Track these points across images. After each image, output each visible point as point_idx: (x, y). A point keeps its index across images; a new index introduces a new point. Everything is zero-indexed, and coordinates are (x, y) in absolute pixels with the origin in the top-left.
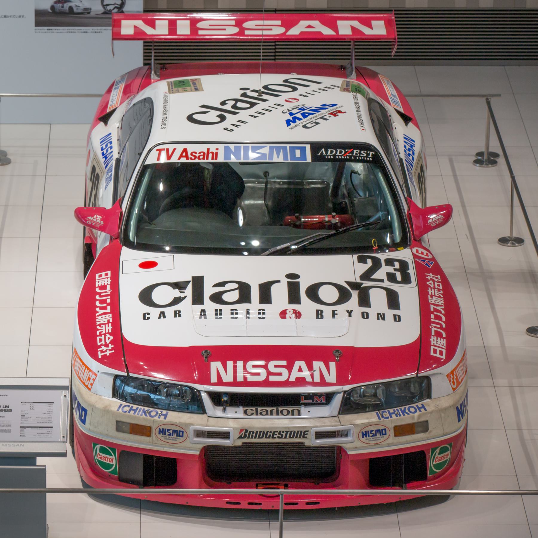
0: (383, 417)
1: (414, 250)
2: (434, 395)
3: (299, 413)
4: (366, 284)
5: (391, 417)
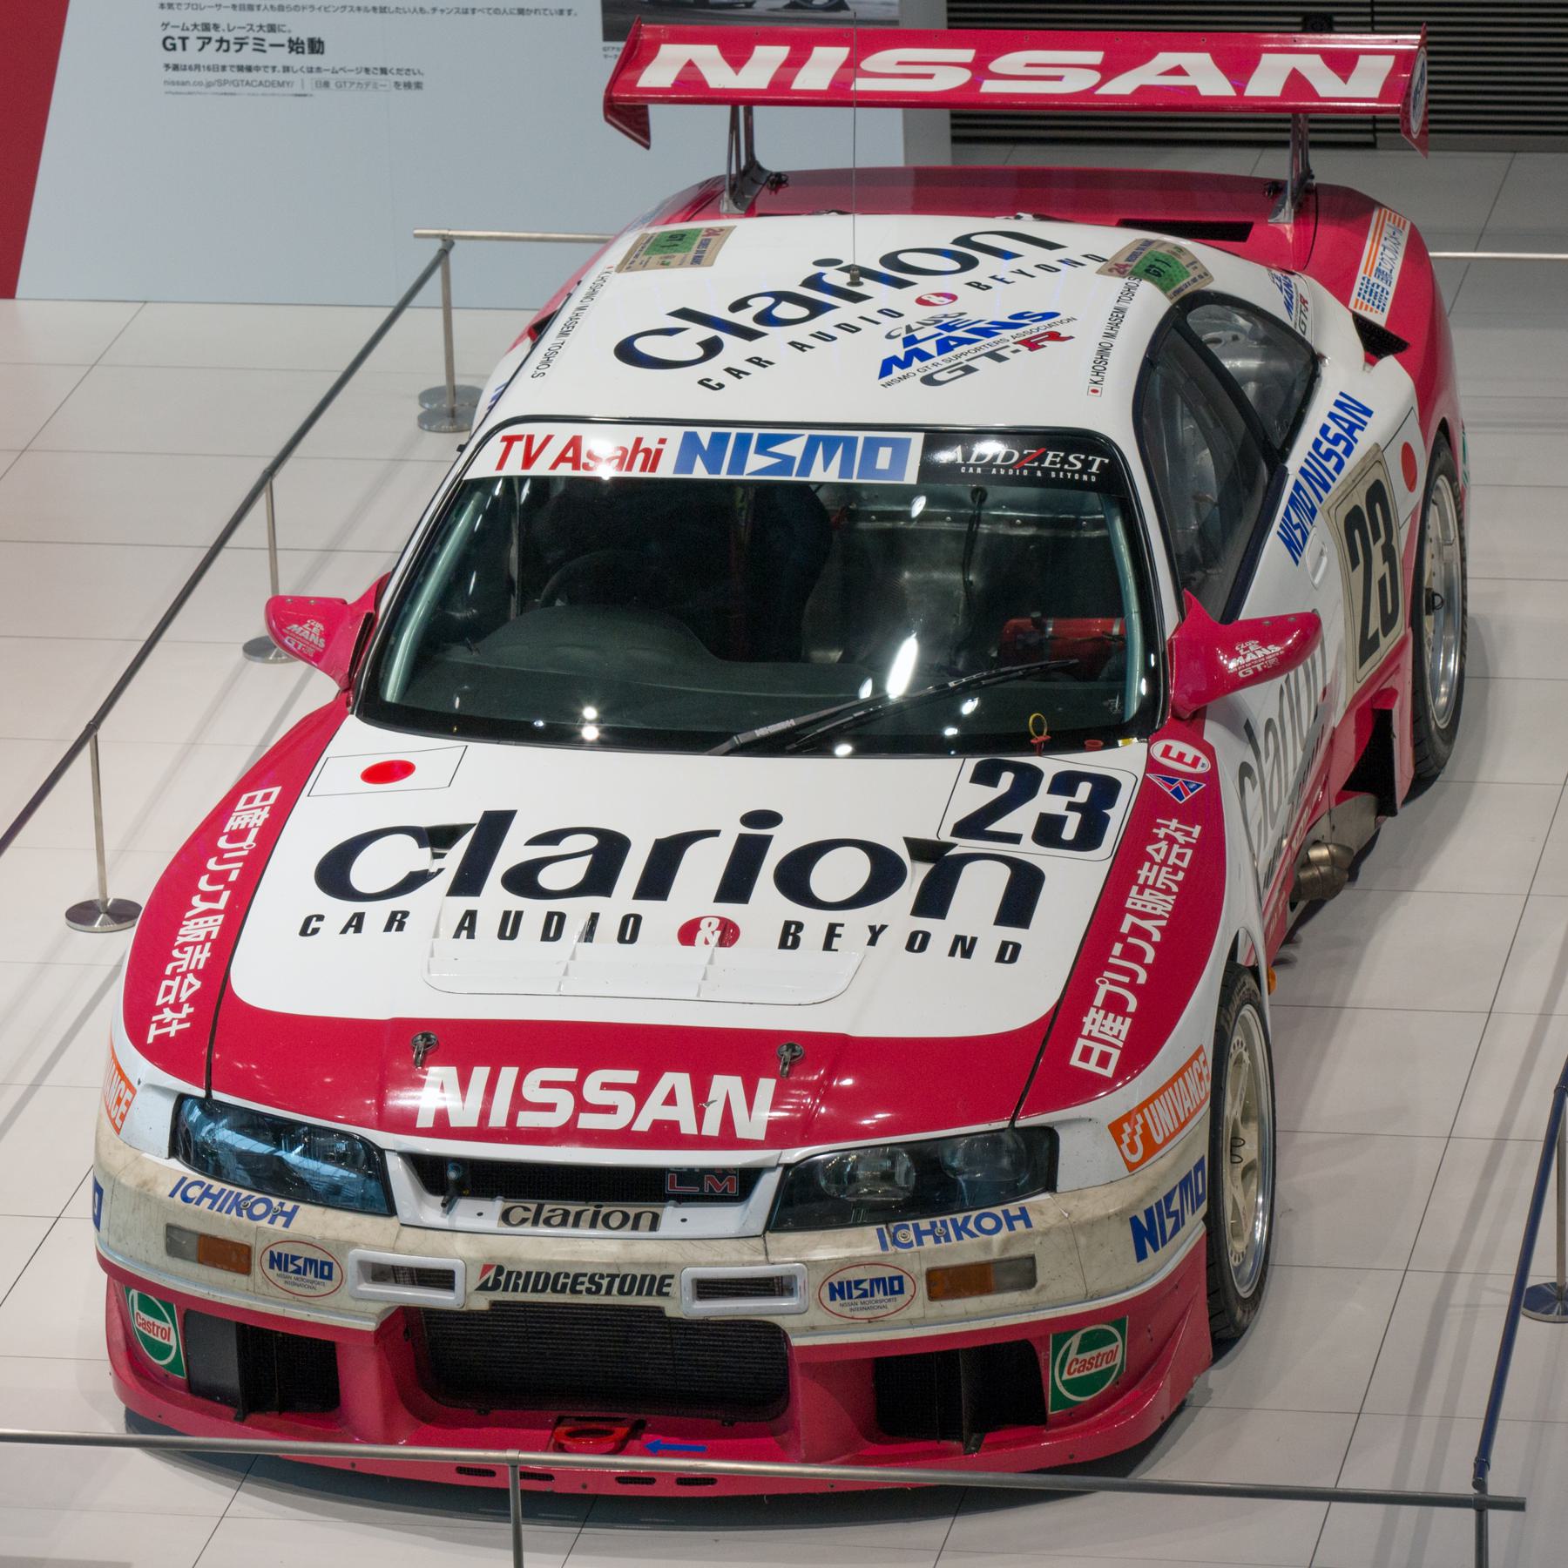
0: (895, 1242)
1: (1158, 748)
2: (1063, 1181)
3: (655, 1219)
4: (964, 846)
5: (920, 1243)
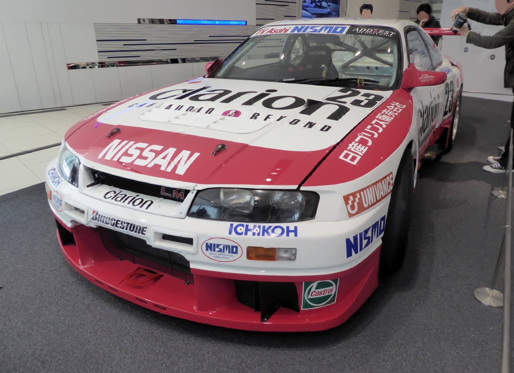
5: (246, 234)
